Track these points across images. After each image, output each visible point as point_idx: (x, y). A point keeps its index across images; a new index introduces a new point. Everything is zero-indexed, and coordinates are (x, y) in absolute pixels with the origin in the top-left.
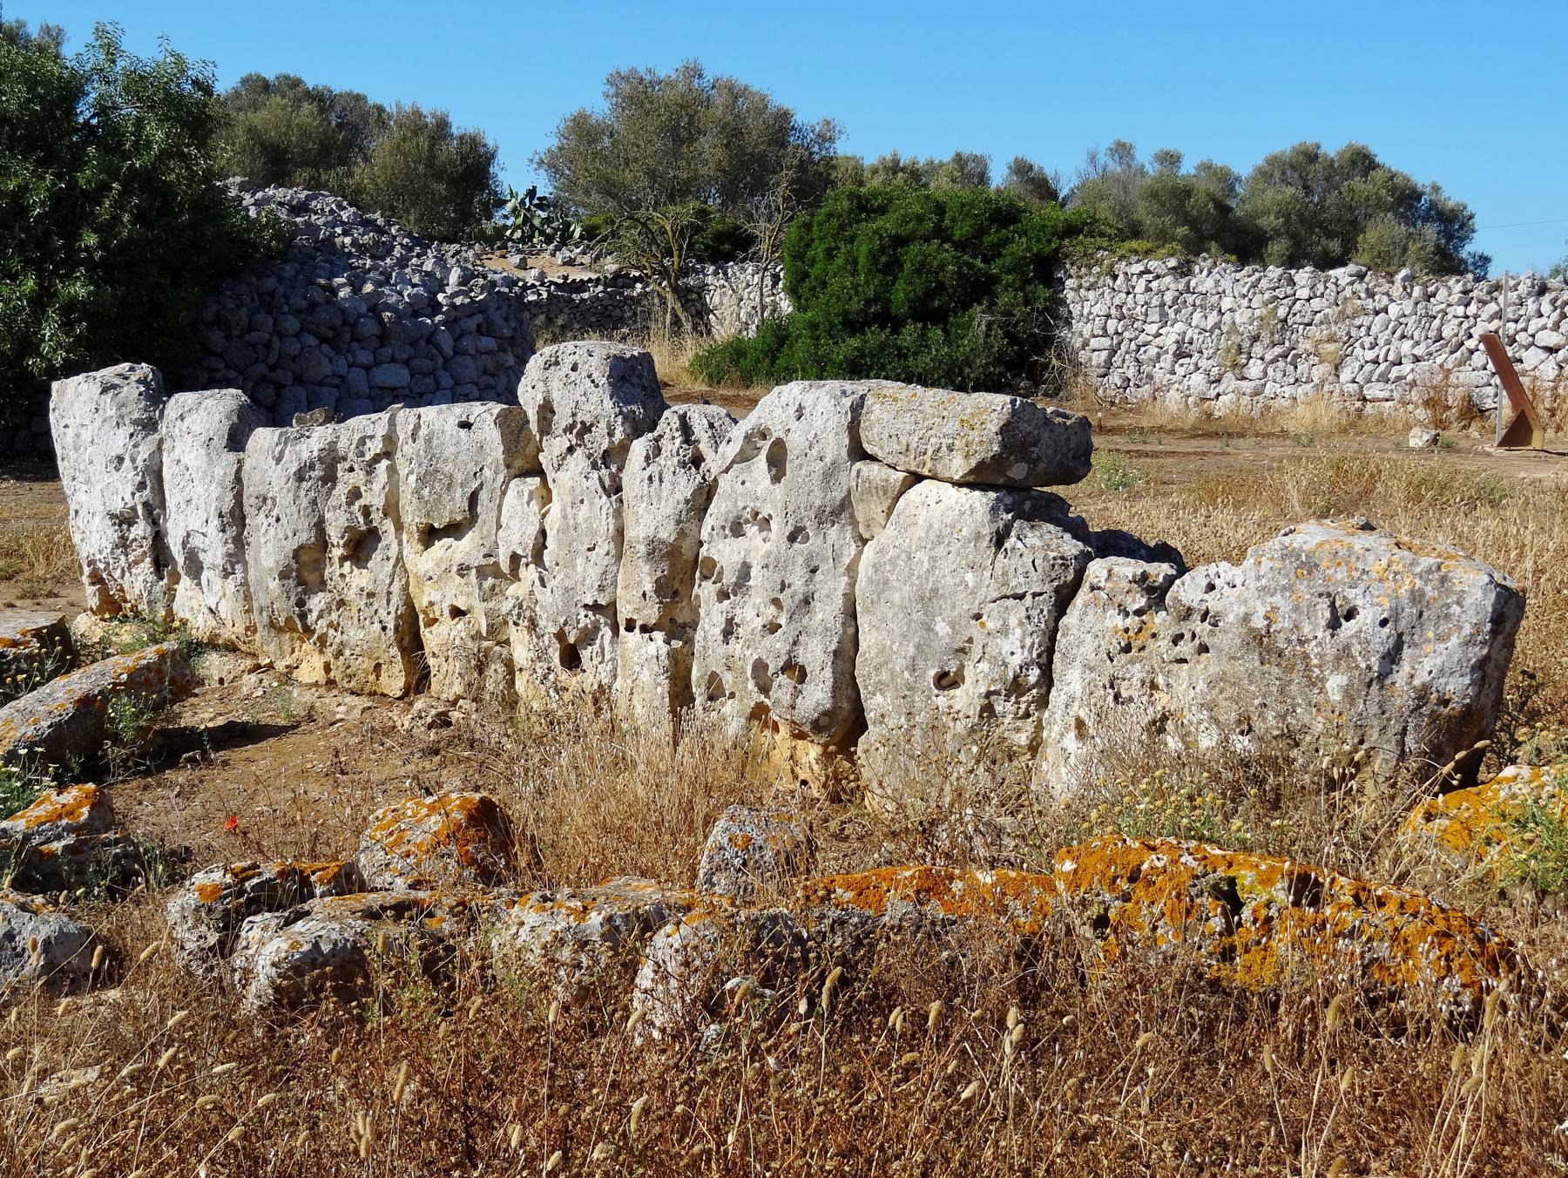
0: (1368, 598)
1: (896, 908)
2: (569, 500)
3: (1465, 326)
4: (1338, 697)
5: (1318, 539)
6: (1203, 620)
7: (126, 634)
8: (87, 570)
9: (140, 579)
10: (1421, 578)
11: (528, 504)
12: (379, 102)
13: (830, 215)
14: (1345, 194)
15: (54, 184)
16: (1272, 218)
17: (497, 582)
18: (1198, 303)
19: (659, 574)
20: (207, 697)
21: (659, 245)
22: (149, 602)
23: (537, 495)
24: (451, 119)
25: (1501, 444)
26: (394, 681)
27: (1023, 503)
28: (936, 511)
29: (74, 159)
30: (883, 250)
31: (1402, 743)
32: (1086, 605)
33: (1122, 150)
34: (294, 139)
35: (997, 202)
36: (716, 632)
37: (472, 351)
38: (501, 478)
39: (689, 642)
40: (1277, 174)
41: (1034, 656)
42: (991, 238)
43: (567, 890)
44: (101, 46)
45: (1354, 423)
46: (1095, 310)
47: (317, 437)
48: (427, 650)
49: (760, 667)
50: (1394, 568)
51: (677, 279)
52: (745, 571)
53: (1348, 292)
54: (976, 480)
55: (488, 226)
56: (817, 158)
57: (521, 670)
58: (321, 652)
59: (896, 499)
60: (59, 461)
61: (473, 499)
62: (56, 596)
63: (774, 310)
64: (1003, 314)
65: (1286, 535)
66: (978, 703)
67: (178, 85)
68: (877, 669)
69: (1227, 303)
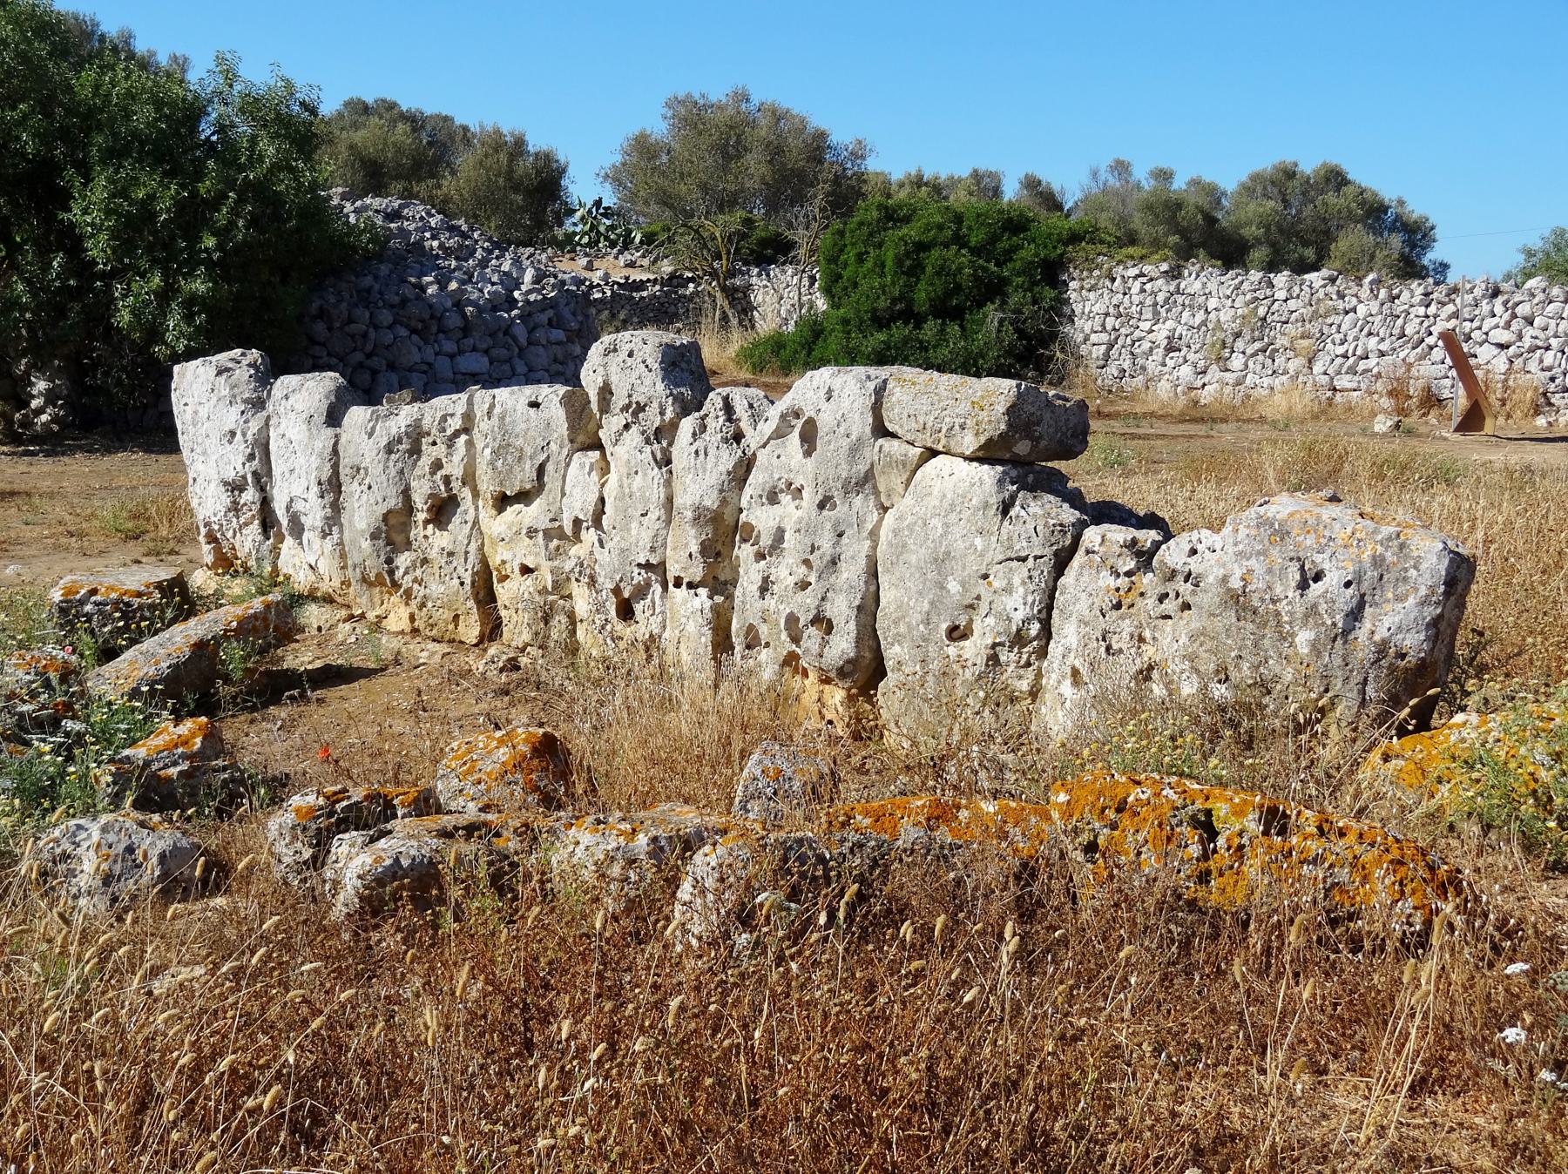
1: (909, 833)
2: (624, 471)
3: (1426, 324)
4: (1306, 651)
5: (1290, 509)
6: (1185, 582)
7: (237, 587)
9: (250, 538)
11: (589, 474)
12: (465, 122)
13: (861, 224)
15: (178, 193)
16: (1254, 228)
18: (1187, 302)
19: (704, 537)
22: (257, 559)
24: (527, 138)
25: (1457, 430)
26: (470, 630)
27: (1026, 476)
28: (949, 483)
29: (196, 172)
30: (907, 254)
32: (1082, 567)
33: (1121, 168)
34: (390, 155)
38: (565, 451)
39: (730, 597)
40: (1259, 189)
42: (1003, 245)
43: (618, 814)
44: (220, 72)
45: (1325, 410)
47: (404, 415)
48: (499, 603)
49: (792, 620)
50: (1358, 535)
51: (725, 279)
53: (1321, 294)
54: (985, 456)
55: (559, 233)
56: (850, 173)
58: (407, 604)
59: (914, 472)
61: (541, 470)
62: (177, 553)
64: (1014, 312)
66: (985, 653)
68: (895, 623)
69: (1212, 303)
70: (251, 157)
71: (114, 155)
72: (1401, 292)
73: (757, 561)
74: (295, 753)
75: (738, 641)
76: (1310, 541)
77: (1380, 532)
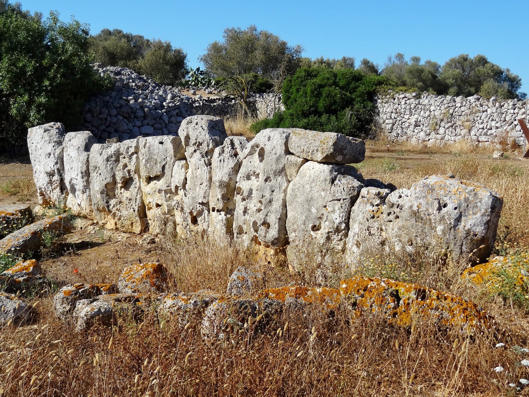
0: (451, 200)
1: (289, 299)
2: (194, 168)
3: (514, 116)
4: (440, 233)
5: (435, 180)
6: (397, 208)
7: (51, 212)
8: (39, 191)
9: (56, 194)
10: (468, 194)
11: (181, 169)
12: (148, 38)
13: (298, 77)
14: (477, 72)
15: (35, 64)
16: (451, 80)
17: (171, 195)
18: (422, 108)
19: (223, 192)
20: (76, 233)
21: (240, 87)
22: (59, 202)
23: (184, 166)
24: (171, 44)
25: (525, 157)
26: (137, 228)
27: (341, 169)
28: (312, 171)
29: (42, 56)
30: (315, 89)
31: (462, 249)
32: (360, 203)
33: (400, 56)
34: (118, 51)
35: (355, 73)
36: (241, 212)
37: (175, 122)
38: (173, 160)
39: (233, 215)
40: (453, 65)
41: (343, 220)
42: (352, 85)
43: (183, 293)
44: (52, 19)
45: (475, 149)
46: (388, 110)
47: (113, 147)
48: (148, 218)
49: (255, 223)
50: (459, 190)
51: (246, 99)
52: (251, 192)
53: (474, 105)
54: (325, 161)
55: (183, 81)
56: (295, 58)
57: (178, 224)
58: (114, 219)
59: (300, 168)
60: (30, 155)
61: (163, 168)
62: (30, 200)
63: (279, 110)
64: (356, 111)
65: (425, 179)
66: (325, 236)
67: (77, 32)
68: (293, 224)
69: (432, 108)
70: (63, 51)
71: (11, 50)
72: (504, 104)
73: (242, 201)
74: (69, 274)
75: (235, 232)
76: (442, 192)
77: (467, 189)
